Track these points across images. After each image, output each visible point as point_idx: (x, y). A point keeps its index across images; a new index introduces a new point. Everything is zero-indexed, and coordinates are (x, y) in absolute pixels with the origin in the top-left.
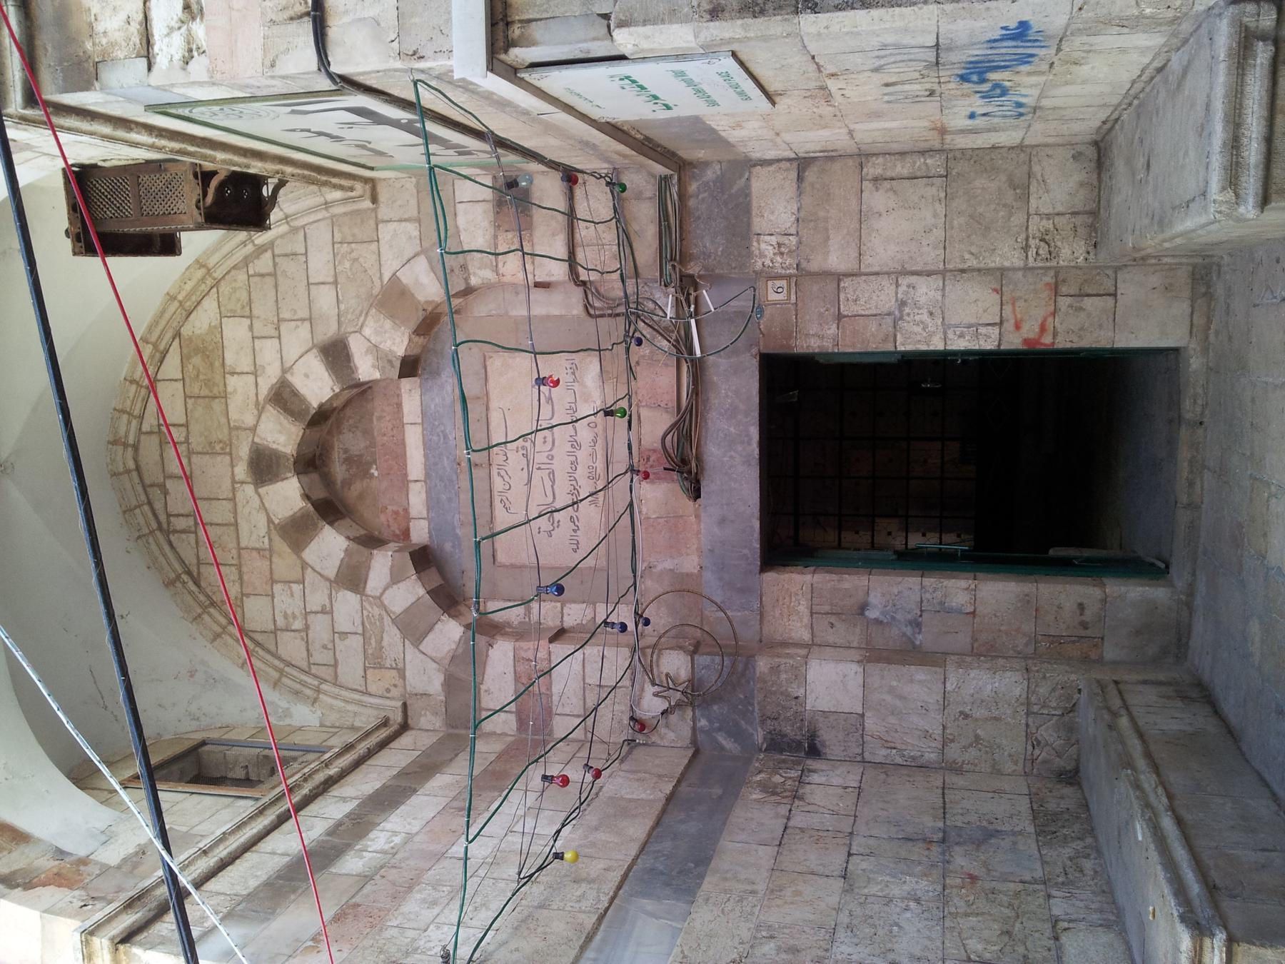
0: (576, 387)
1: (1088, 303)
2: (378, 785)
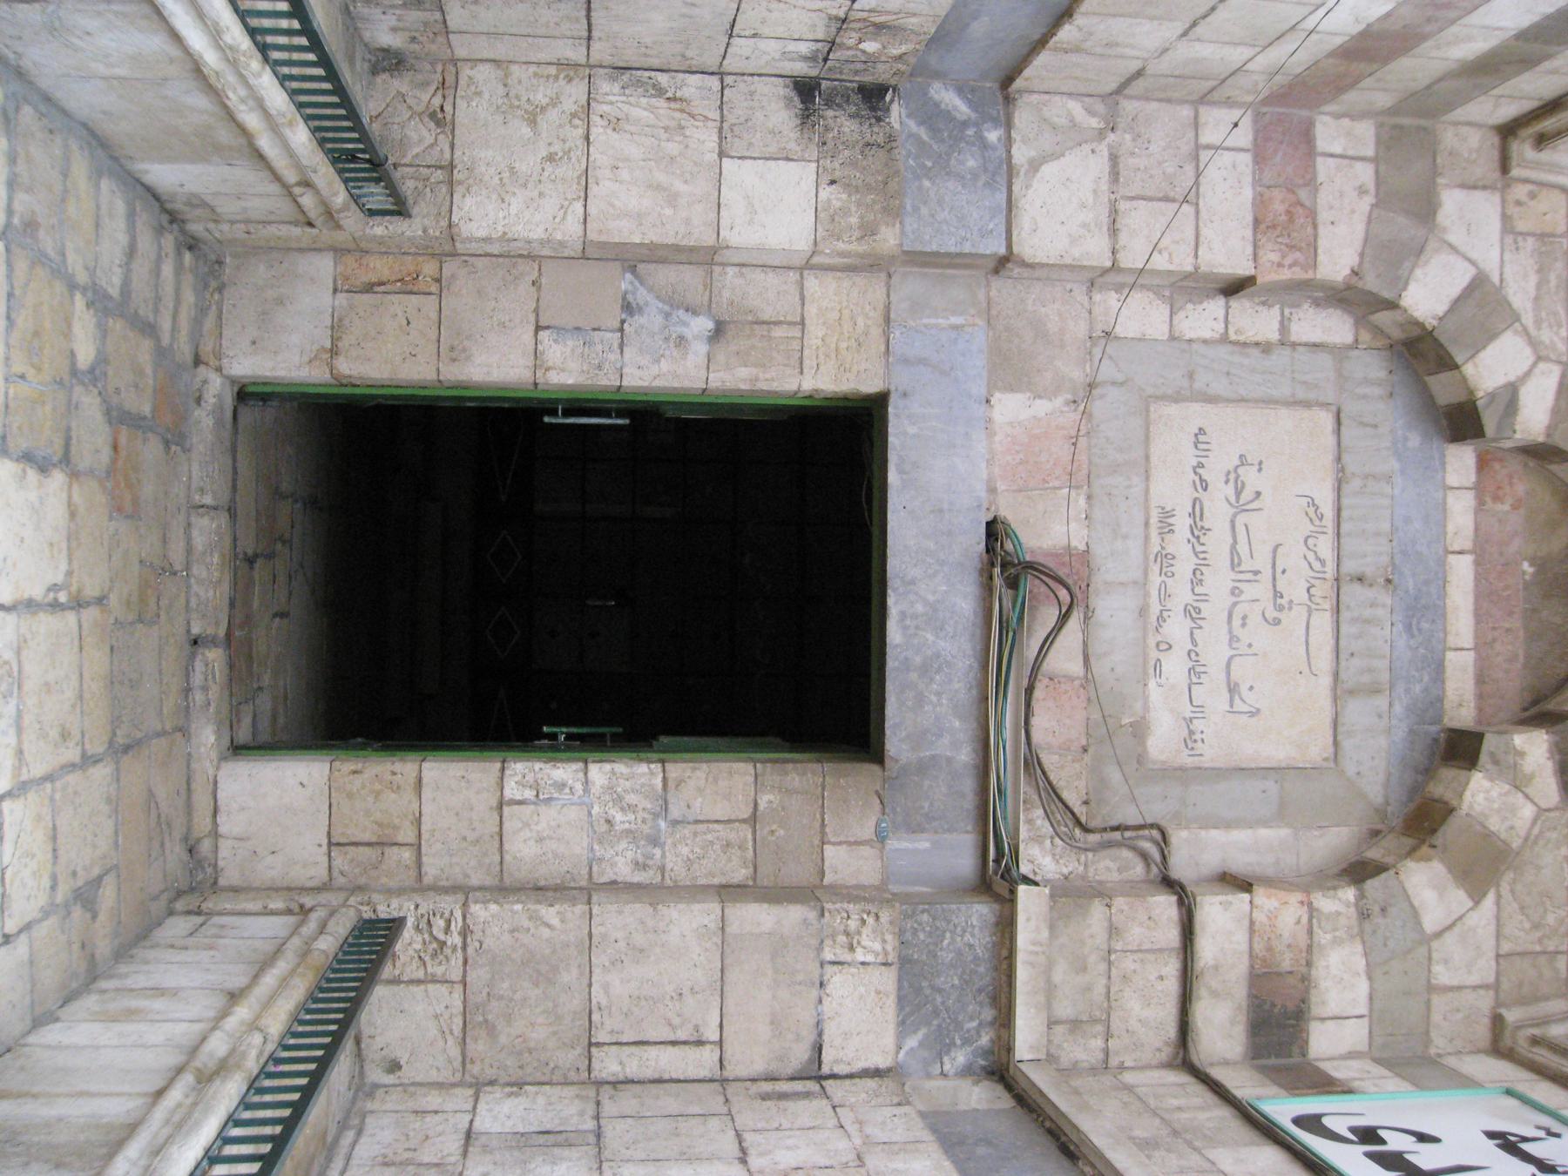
0: (1187, 711)
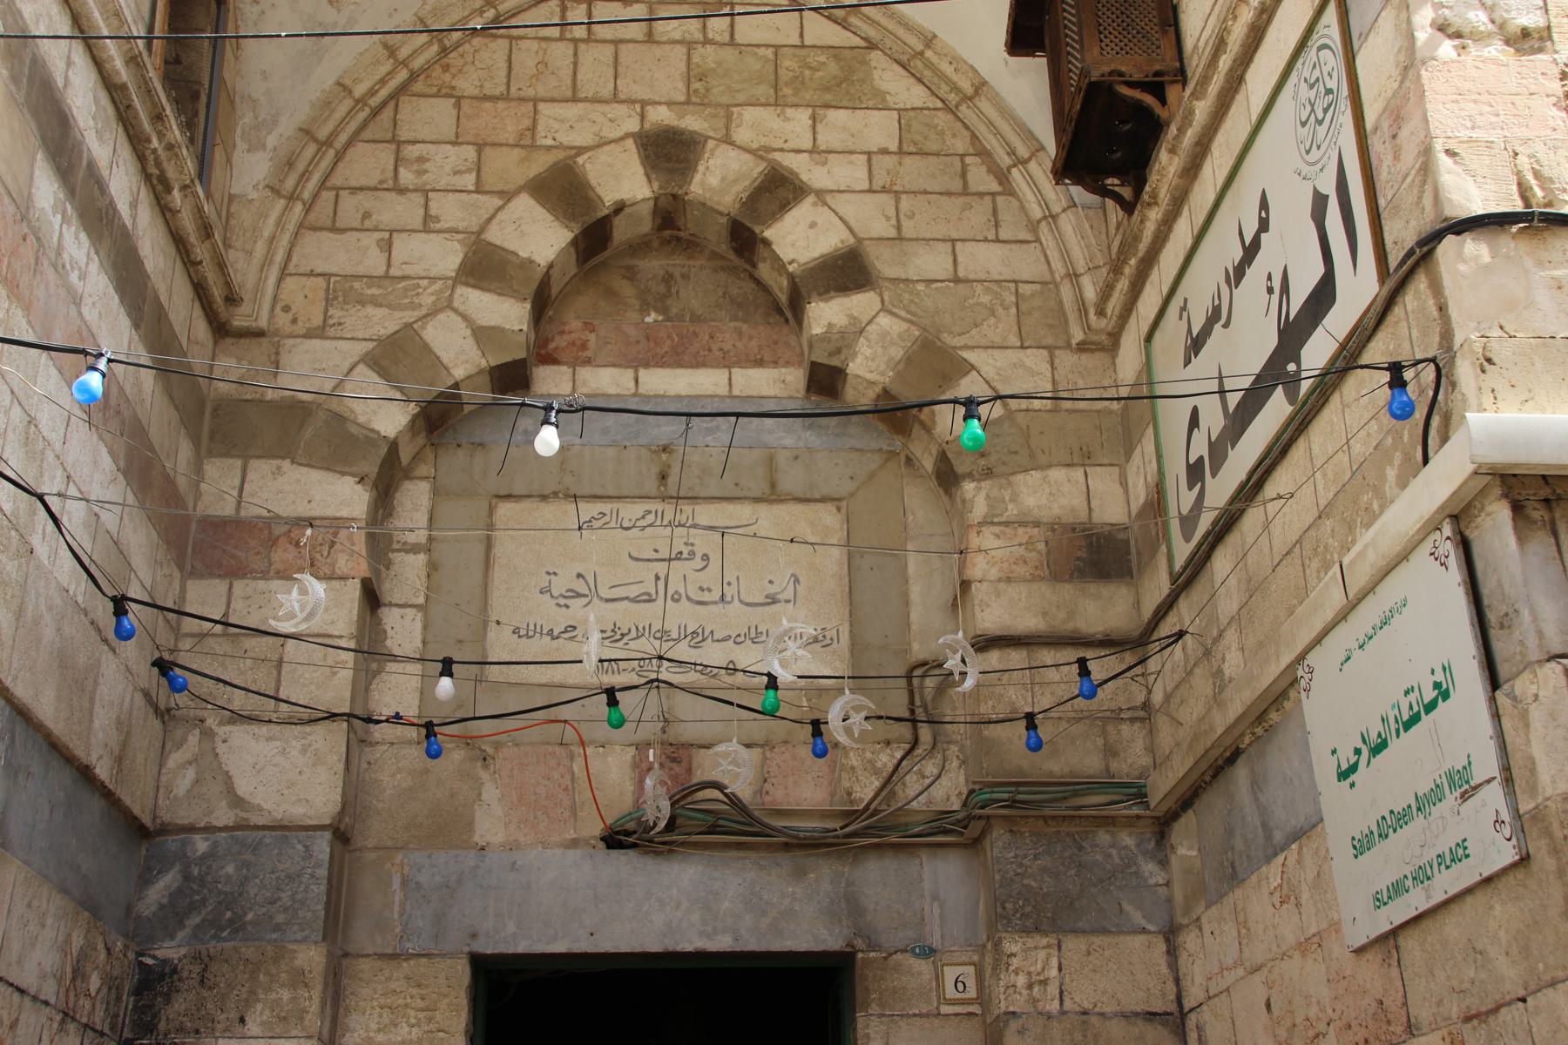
2: (149, 266)
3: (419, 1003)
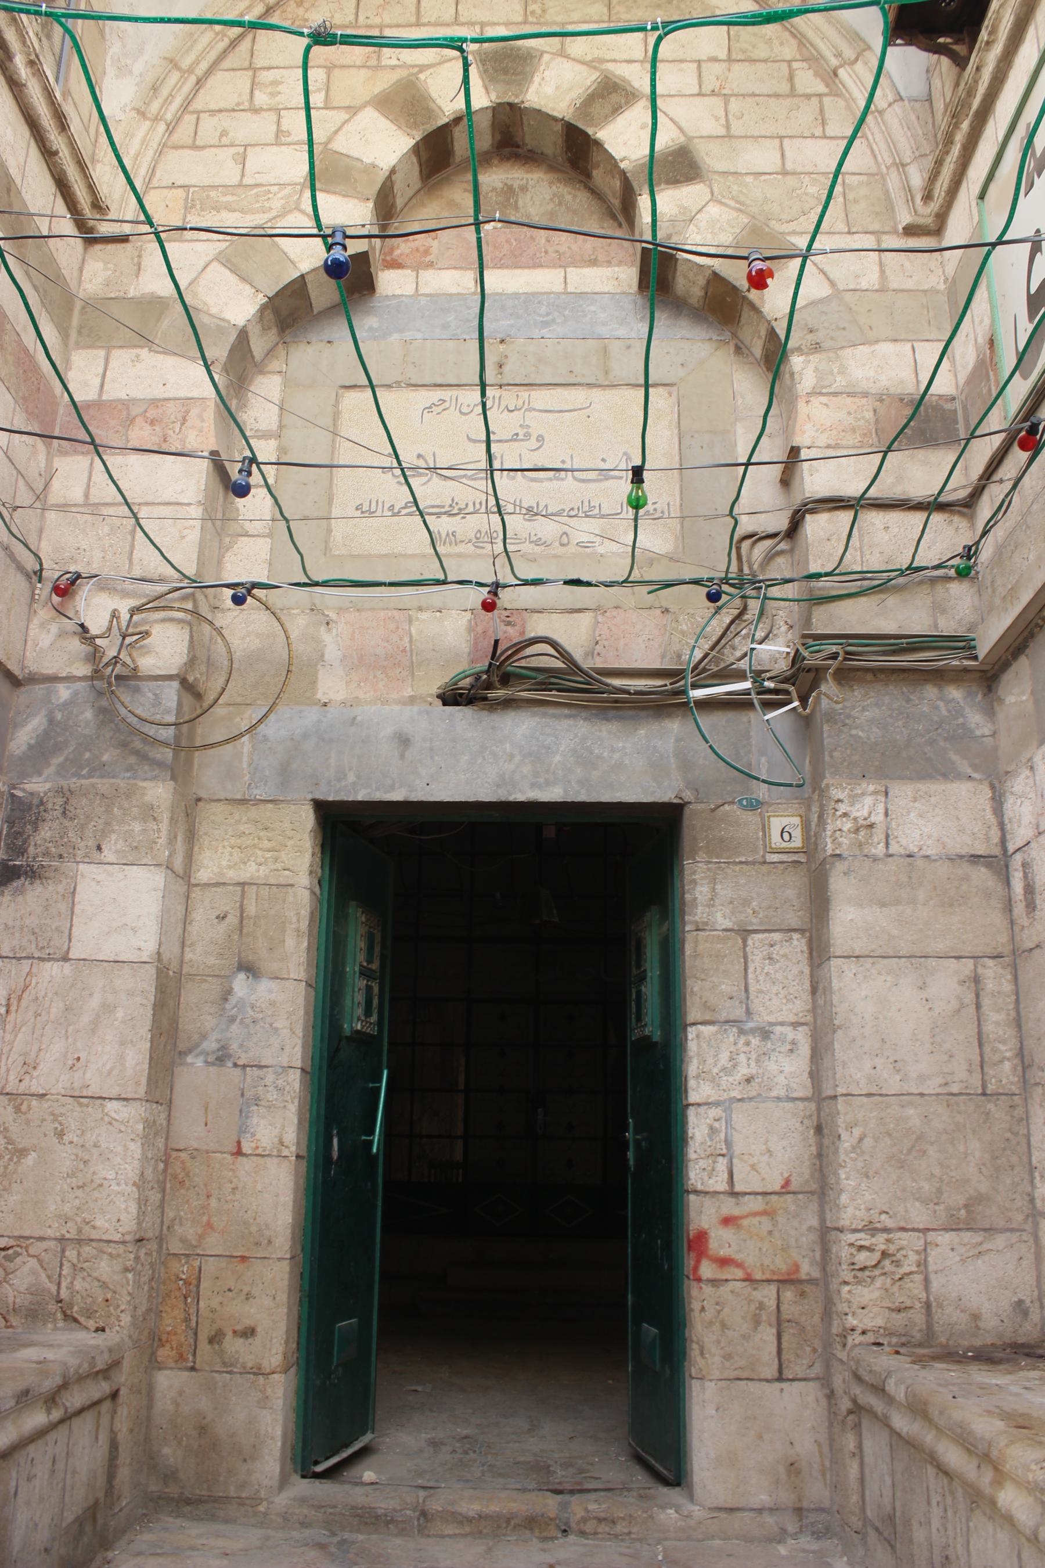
1: (768, 1334)
3: (267, 844)
